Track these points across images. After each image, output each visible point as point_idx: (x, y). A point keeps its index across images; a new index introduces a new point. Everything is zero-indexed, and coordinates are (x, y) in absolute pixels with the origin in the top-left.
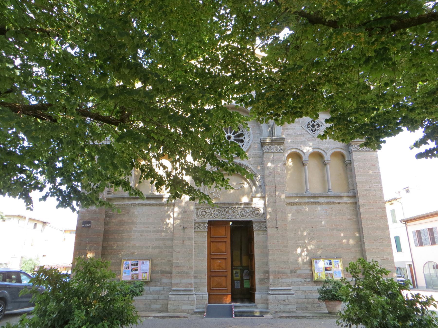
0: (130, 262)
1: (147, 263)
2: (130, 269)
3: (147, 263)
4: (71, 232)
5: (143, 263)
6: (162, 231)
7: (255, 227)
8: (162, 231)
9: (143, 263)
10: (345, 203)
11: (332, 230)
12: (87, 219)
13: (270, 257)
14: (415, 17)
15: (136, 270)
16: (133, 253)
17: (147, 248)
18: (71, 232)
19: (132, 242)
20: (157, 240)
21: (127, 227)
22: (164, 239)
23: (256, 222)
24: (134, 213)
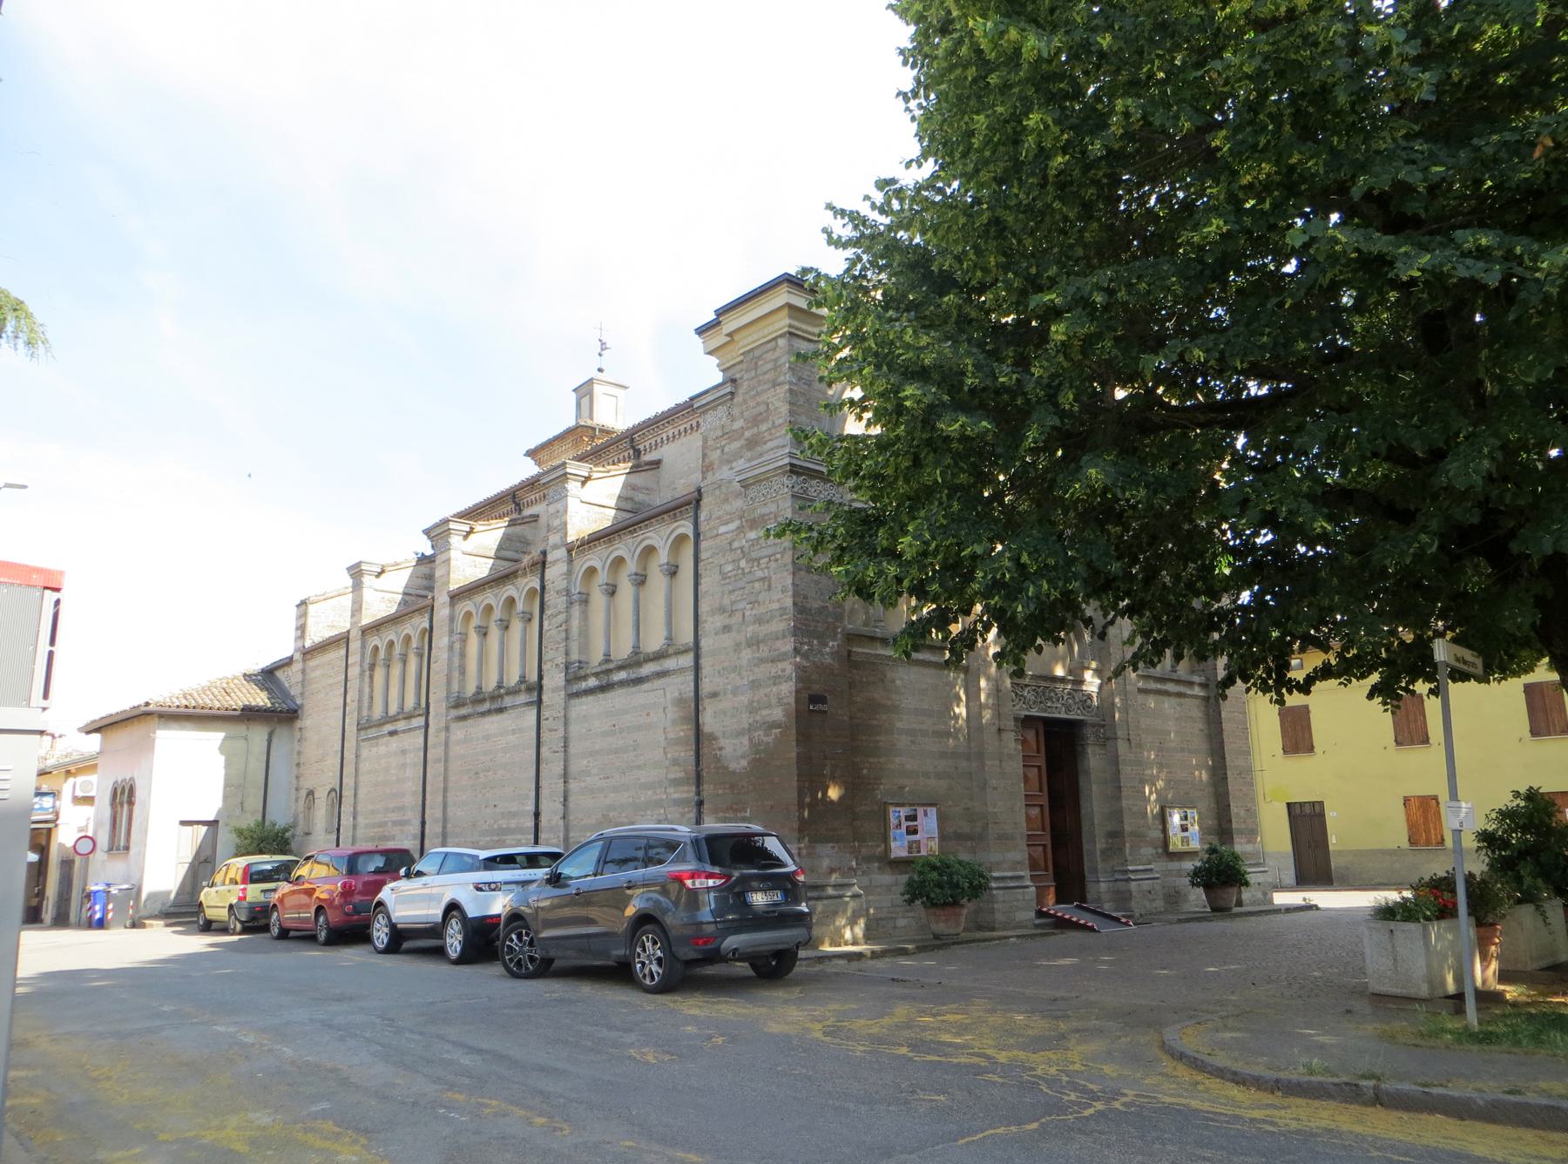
0: (904, 812)
1: (932, 811)
2: (904, 830)
3: (932, 811)
4: (1241, 832)
5: (926, 814)
6: (948, 734)
7: (1088, 732)
8: (948, 734)
9: (926, 814)
10: (1193, 697)
11: (1182, 750)
12: (817, 688)
13: (1124, 803)
14: (1451, 276)
15: (915, 832)
16: (902, 788)
17: (926, 775)
18: (1241, 832)
19: (897, 760)
20: (943, 755)
21: (884, 717)
22: (954, 755)
23: (1093, 725)
24: (893, 681)
